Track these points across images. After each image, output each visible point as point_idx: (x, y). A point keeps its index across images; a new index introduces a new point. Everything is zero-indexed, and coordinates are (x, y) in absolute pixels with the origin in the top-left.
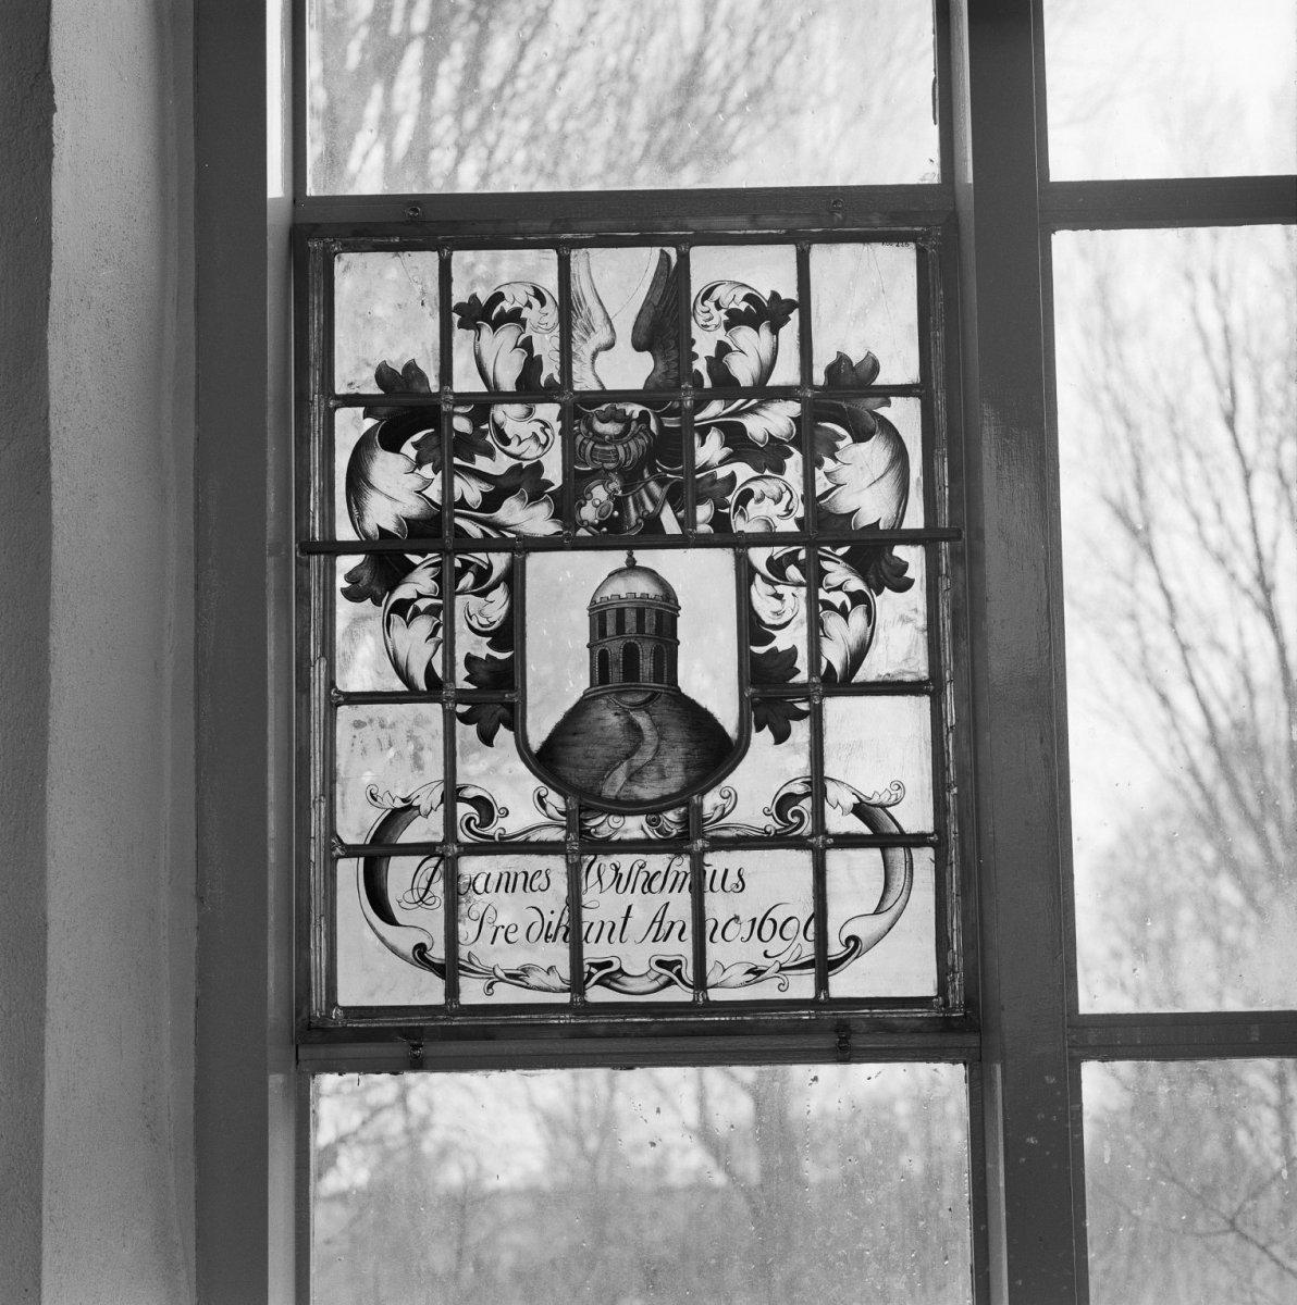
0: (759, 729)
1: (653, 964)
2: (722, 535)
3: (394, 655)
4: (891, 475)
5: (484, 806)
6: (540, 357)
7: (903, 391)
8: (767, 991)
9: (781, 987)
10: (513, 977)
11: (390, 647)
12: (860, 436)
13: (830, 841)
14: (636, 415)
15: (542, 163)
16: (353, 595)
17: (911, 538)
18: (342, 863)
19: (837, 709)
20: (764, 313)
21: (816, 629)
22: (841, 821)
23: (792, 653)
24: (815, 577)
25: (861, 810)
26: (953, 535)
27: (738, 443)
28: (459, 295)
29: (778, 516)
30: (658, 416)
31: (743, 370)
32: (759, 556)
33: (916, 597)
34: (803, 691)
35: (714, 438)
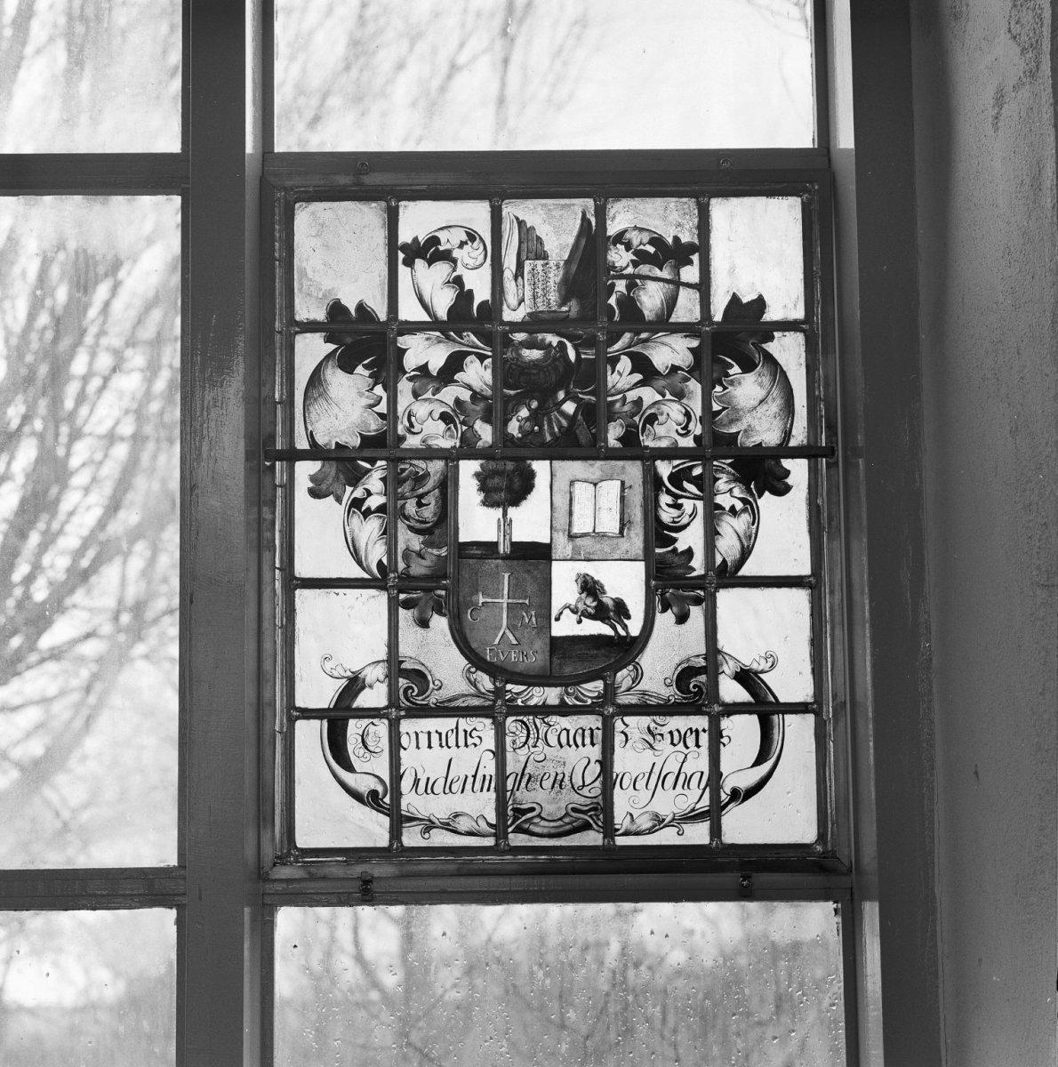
0: (664, 610)
1: (570, 811)
2: (631, 447)
3: (354, 546)
4: (775, 392)
5: (419, 677)
6: (471, 291)
7: (787, 326)
8: (667, 837)
9: (680, 833)
10: (448, 827)
12: (748, 367)
13: (403, 713)
14: (555, 344)
16: (315, 493)
17: (796, 453)
18: (300, 724)
19: (727, 599)
20: (670, 254)
21: (711, 534)
22: (731, 691)
23: (689, 553)
24: (706, 486)
25: (745, 677)
26: (829, 452)
27: (643, 366)
28: (405, 236)
29: (667, 504)
30: (576, 347)
31: (651, 298)
32: (665, 469)
33: (798, 495)
34: (700, 582)
35: (625, 364)
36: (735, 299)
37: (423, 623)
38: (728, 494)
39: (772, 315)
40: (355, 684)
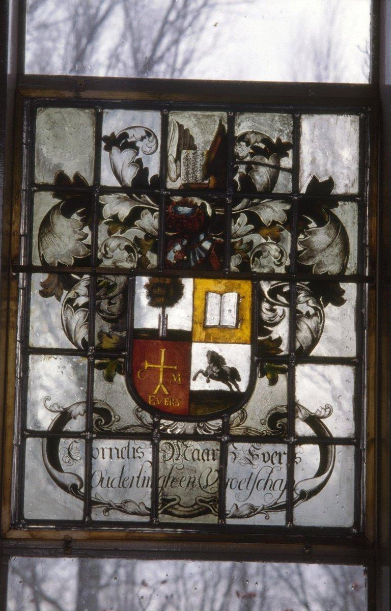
0: (262, 376)
2: (245, 272)
7: (347, 198)
8: (258, 520)
9: (267, 518)
10: (120, 508)
11: (64, 320)
15: (257, 171)
16: (44, 294)
20: (276, 149)
21: (294, 329)
22: (303, 428)
23: (279, 341)
24: (292, 299)
27: (257, 224)
28: (106, 131)
34: (285, 359)
39: (339, 189)
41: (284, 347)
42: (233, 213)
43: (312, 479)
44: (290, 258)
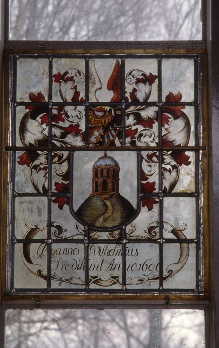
0: (143, 206)
2: (133, 147)
3: (33, 182)
9: (149, 285)
12: (176, 117)
14: (108, 110)
17: (191, 149)
19: (168, 201)
20: (148, 79)
21: (161, 176)
23: (154, 183)
24: (161, 161)
27: (139, 119)
28: (55, 72)
30: (114, 110)
32: (144, 154)
36: (171, 94)
37: (61, 208)
38: (169, 160)
39: (183, 100)
40: (33, 231)
41: (157, 186)
42: (126, 129)
43: (176, 265)
44: (158, 137)
